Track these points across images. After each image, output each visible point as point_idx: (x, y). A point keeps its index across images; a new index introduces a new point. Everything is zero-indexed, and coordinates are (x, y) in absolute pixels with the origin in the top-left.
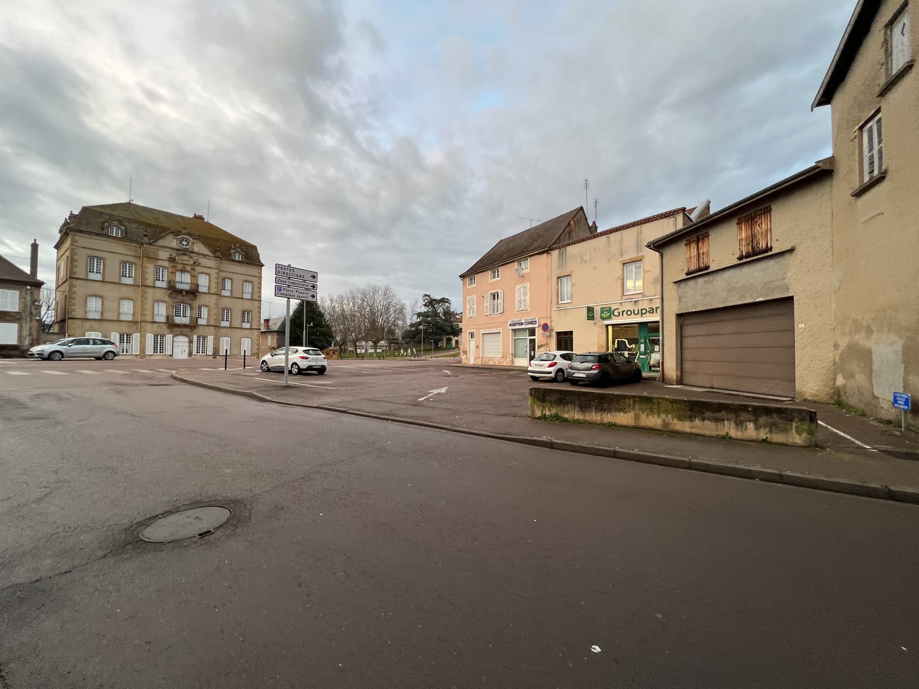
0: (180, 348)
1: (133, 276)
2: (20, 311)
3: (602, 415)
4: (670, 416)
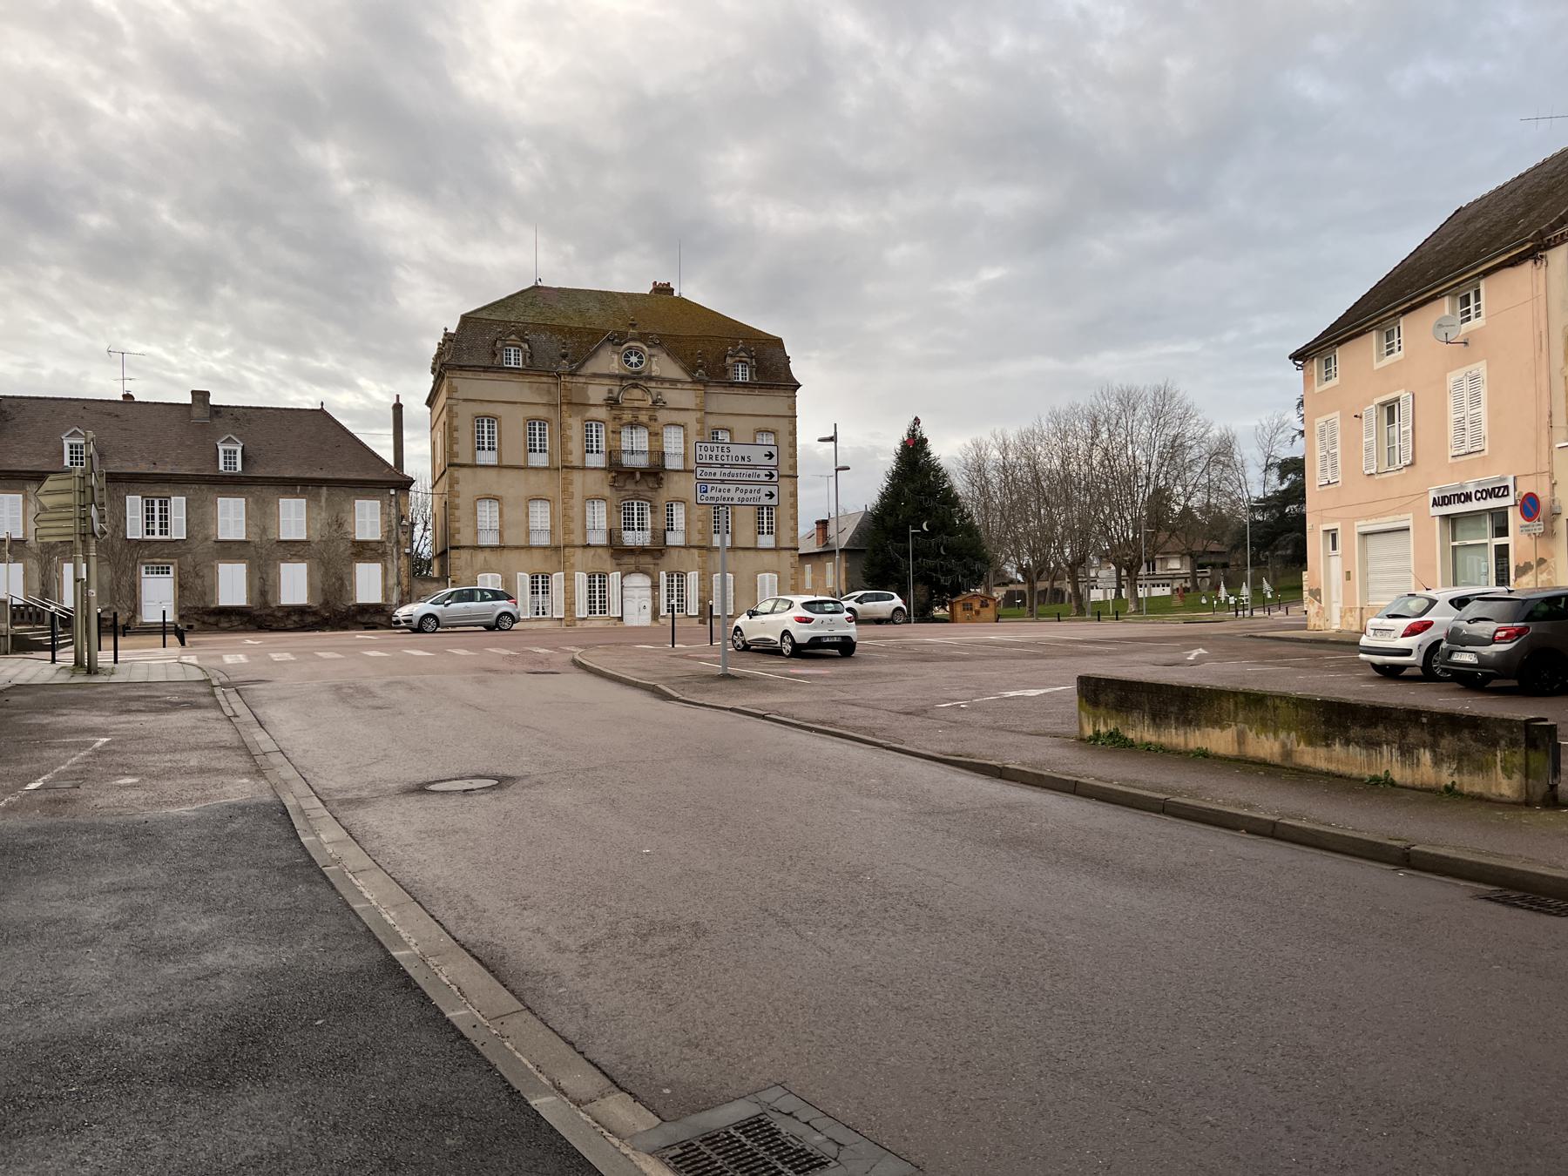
0: (636, 601)
1: (547, 449)
2: (384, 539)
3: (1185, 733)
4: (1293, 734)
